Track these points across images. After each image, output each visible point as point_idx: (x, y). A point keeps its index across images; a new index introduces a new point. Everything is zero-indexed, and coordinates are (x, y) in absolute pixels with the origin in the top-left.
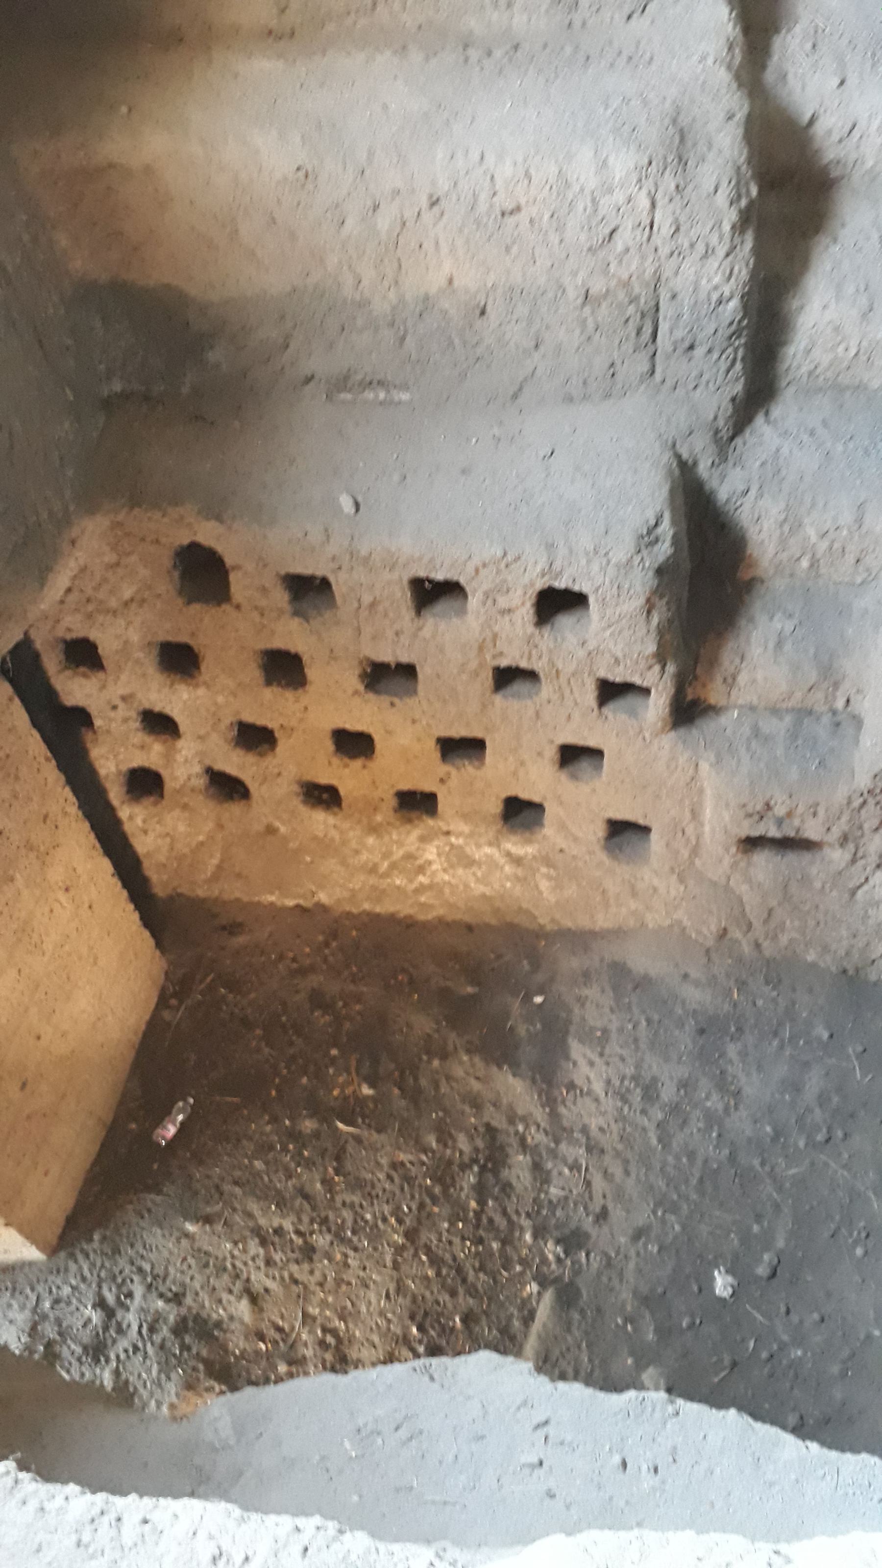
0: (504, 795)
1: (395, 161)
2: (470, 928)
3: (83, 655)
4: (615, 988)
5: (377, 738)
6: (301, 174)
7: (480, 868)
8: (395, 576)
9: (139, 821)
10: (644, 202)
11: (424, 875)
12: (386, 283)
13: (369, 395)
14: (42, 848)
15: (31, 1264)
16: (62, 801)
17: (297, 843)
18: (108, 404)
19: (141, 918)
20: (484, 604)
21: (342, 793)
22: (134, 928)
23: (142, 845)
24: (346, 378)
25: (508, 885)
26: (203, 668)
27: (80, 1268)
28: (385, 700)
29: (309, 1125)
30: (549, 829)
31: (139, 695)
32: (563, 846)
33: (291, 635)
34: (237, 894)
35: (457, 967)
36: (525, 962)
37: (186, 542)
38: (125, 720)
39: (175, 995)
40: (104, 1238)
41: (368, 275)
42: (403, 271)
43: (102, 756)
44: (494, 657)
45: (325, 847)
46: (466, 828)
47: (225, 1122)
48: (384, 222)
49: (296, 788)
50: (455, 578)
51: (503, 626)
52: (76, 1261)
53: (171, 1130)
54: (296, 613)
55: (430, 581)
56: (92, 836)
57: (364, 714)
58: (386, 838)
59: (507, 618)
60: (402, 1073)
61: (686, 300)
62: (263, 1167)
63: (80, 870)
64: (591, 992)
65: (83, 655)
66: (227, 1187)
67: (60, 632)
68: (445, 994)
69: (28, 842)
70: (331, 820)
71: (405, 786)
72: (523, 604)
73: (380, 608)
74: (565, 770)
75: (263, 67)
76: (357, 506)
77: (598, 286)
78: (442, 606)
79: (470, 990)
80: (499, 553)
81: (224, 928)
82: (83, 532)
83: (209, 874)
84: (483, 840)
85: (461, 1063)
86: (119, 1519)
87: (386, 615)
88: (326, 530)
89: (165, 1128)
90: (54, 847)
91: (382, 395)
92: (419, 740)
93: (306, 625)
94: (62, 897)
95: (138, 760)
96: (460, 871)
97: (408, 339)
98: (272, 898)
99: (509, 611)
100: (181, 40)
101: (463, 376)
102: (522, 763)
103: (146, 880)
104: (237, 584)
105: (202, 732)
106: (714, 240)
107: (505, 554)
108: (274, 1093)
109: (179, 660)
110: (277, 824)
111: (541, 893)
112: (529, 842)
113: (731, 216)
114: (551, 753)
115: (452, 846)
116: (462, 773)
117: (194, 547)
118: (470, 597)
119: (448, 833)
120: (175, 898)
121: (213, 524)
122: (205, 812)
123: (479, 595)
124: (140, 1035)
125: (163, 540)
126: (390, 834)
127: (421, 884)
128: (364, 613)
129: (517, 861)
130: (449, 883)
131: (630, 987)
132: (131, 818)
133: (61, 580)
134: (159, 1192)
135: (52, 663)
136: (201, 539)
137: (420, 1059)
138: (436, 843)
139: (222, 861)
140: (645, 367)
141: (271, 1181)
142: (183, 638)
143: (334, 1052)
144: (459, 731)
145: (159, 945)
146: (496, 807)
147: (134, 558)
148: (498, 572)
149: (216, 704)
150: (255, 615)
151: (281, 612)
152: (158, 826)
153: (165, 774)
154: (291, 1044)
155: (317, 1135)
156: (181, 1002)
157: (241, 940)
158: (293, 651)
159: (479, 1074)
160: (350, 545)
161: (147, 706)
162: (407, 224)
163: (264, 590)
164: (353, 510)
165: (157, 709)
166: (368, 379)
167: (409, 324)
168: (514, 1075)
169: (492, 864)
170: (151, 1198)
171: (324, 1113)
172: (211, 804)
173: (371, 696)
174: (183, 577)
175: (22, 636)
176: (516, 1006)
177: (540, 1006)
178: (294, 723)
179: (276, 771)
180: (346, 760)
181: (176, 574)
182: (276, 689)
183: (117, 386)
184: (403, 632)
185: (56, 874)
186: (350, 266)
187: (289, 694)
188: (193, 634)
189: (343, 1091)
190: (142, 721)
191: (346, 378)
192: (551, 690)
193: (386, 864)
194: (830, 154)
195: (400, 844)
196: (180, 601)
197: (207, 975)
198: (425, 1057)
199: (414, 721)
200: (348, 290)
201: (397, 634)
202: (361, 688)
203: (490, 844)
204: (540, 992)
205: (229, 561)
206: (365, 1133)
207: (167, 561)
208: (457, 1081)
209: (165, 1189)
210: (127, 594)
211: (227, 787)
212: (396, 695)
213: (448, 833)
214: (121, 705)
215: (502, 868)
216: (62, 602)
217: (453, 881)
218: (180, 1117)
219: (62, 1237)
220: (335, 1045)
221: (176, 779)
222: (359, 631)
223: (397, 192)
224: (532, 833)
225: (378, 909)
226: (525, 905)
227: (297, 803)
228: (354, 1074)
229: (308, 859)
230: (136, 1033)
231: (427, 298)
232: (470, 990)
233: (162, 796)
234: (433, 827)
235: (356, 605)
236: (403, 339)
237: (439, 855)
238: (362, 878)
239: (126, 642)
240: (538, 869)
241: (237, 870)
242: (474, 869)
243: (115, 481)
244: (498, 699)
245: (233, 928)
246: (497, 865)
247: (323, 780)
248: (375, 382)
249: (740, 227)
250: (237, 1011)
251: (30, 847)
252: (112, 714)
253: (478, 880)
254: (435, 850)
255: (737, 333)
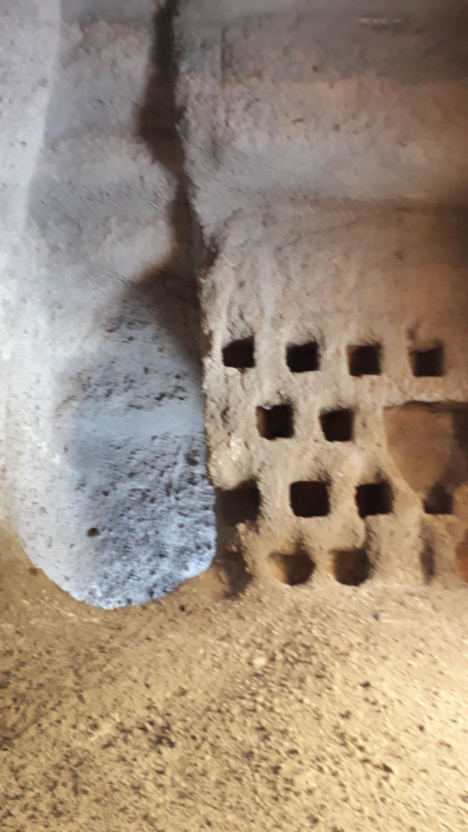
10: (232, 123)
13: (383, 21)
48: (364, 118)
61: (207, 73)
75: (413, 195)
77: (254, 81)
86: (131, 339)
106: (196, 103)
113: (189, 115)
140: (228, 35)
194: (142, 146)
223: (356, 133)
230: (335, 501)
249: (184, 109)
255: (180, 53)
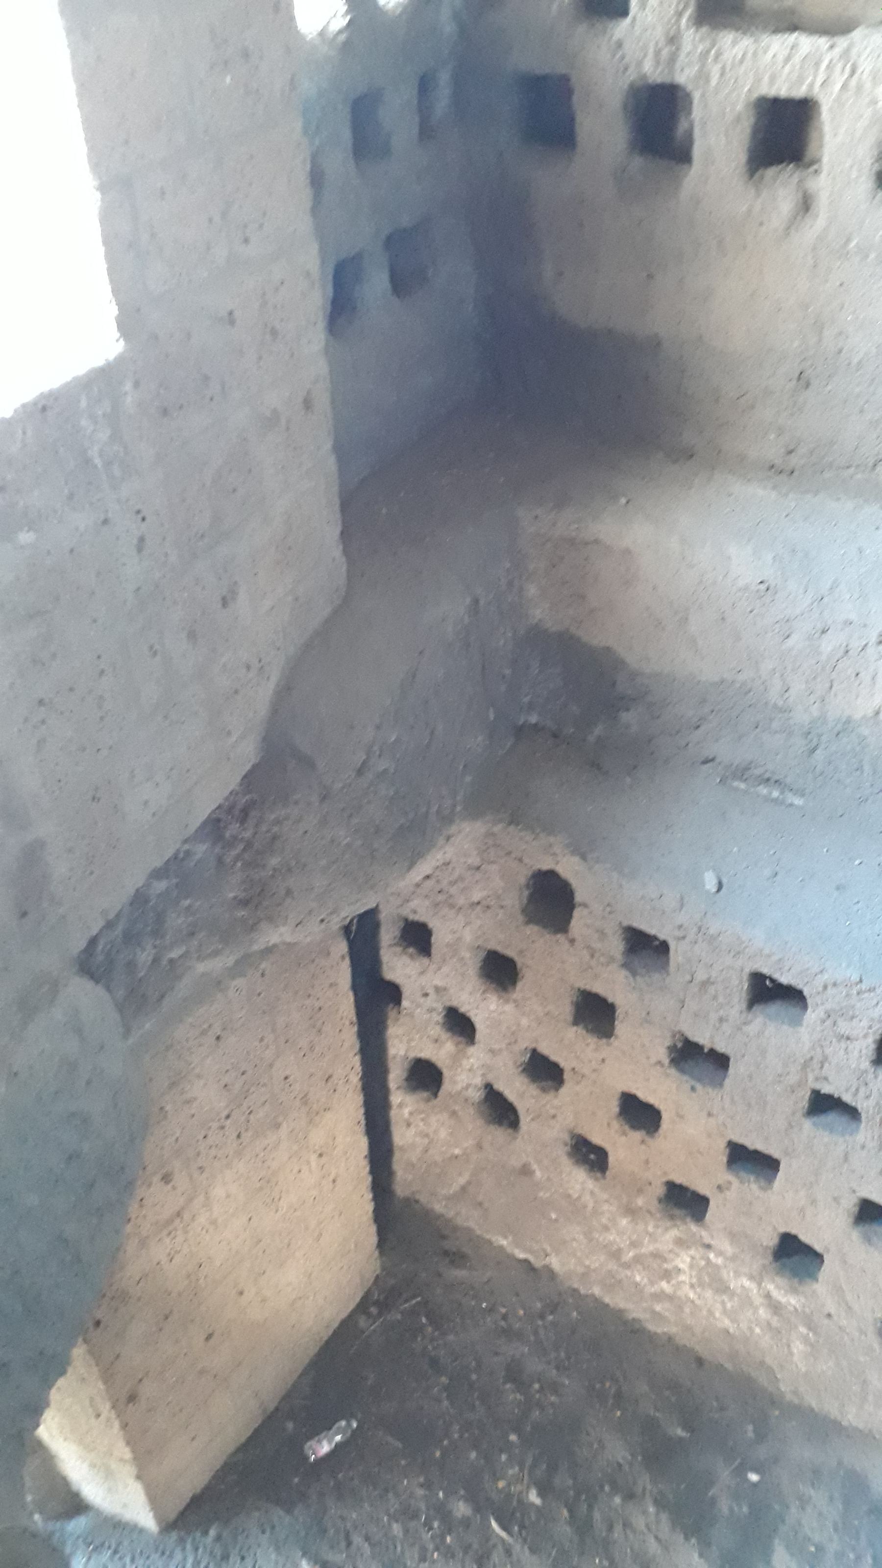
0: (783, 1230)
1: (856, 596)
2: (700, 1361)
3: (417, 937)
4: (847, 1502)
5: (665, 1116)
6: (763, 587)
7: (731, 1299)
8: (739, 963)
9: (406, 1111)
11: (668, 1282)
12: (812, 698)
13: (763, 790)
14: (315, 1106)
15: (142, 1531)
16: (349, 1068)
17: (548, 1195)
18: (520, 731)
19: (374, 1211)
20: (823, 1021)
21: (611, 1159)
22: (365, 1218)
23: (401, 1136)
24: (747, 769)
25: (758, 1330)
26: (520, 985)
27: (185, 1559)
28: (686, 1081)
29: (461, 1509)
30: (821, 1287)
31: (452, 991)
32: (833, 1312)
33: (615, 984)
34: (471, 1224)
35: (673, 1399)
36: (750, 1428)
37: (545, 867)
38: (431, 1010)
39: (376, 1303)
40: (218, 1538)
41: (798, 687)
42: (832, 693)
43: (397, 1036)
44: (817, 1079)
45: (575, 1209)
46: (728, 1248)
47: (380, 1464)
48: (828, 645)
49: (566, 1137)
50: (800, 986)
51: (836, 1051)
52: (184, 1549)
53: (325, 1448)
54: (625, 965)
55: (773, 980)
56: (362, 1111)
57: (661, 1088)
58: (641, 1227)
59: (843, 1045)
60: (578, 1494)
62: (401, 1535)
63: (339, 1140)
64: (818, 1497)
65: (417, 937)
66: (357, 1540)
67: (406, 912)
68: (650, 1426)
69: (306, 1095)
70: (590, 1184)
71: (679, 1179)
72: (865, 1036)
73: (712, 990)
74: (860, 1228)
75: (758, 494)
76: (720, 886)
78: (775, 1008)
79: (680, 1432)
80: (855, 978)
81: (446, 1253)
82: (460, 832)
83: (451, 1192)
84: (746, 1270)
85: (645, 1512)
87: (715, 998)
88: (682, 899)
89: (319, 1441)
90: (325, 1110)
91: (775, 794)
92: (709, 1136)
93: (631, 979)
94: (313, 1158)
95: (427, 1052)
96: (709, 1294)
97: (818, 752)
98: (504, 1243)
99: (848, 1038)
100: (692, 456)
101: (863, 800)
102: (814, 1202)
103: (391, 1173)
104: (579, 922)
105: (496, 1047)
107: (861, 981)
108: (438, 1454)
109: (500, 971)
110: (535, 1167)
111: (791, 1354)
112: (794, 1291)
114: (850, 1204)
115: (708, 1260)
116: (743, 1187)
117: (551, 875)
118: (810, 1010)
119: (708, 1247)
120: (410, 1202)
121: (576, 859)
122: (470, 1127)
123: (820, 1012)
124: (330, 1332)
125: (526, 860)
126: (646, 1224)
127: (663, 1292)
128: (694, 988)
129: (776, 1308)
130: (693, 1302)
131: (865, 1508)
132: (400, 1106)
133: (425, 867)
134: (289, 1511)
135: (388, 935)
136: (560, 870)
137: (602, 1487)
138: (692, 1252)
139: (469, 1183)
141: (403, 1552)
142: (510, 953)
143: (513, 1437)
144: (754, 1143)
145: (381, 1245)
146: (772, 1241)
147: (494, 868)
148: (848, 995)
149: (519, 1025)
150: (585, 953)
151: (612, 959)
152: (421, 1124)
153: (446, 1073)
154: (473, 1408)
155: (466, 1523)
156: (380, 1314)
157: (459, 1274)
158: (610, 1000)
159: (660, 1535)
160: (701, 920)
161: (455, 1003)
162: (850, 653)
163: (602, 934)
164: (714, 890)
165: (462, 1010)
166: (767, 776)
167: (824, 738)
168: (701, 1555)
169: (746, 1301)
170: (278, 1514)
171: (483, 1505)
172: (480, 1122)
173: (673, 1071)
174: (532, 898)
175: (374, 905)
176: (725, 1476)
177: (755, 1485)
178: (586, 1071)
179: (552, 1112)
180: (627, 1127)
181: (526, 893)
182: (580, 1030)
183: (533, 719)
184: (727, 1020)
185: (317, 1137)
186: (782, 675)
187: (592, 1040)
188: (521, 952)
189: (509, 1485)
190: (445, 1016)
191: (747, 769)
192: (869, 1137)
193: (631, 1254)
195: (653, 1237)
196: (521, 918)
197: (414, 1297)
198: (607, 1488)
199: (710, 1115)
200: (774, 695)
201: (721, 1020)
202: (666, 1061)
203: (751, 1278)
204: (756, 1470)
205: (578, 898)
206: (517, 1548)
207: (523, 876)
208: (634, 1531)
209: (296, 1512)
210: (476, 896)
211: (499, 1110)
212: (699, 1080)
213: (708, 1247)
214: (433, 995)
215: (756, 1309)
216: (418, 885)
217: (698, 1302)
218: (338, 1438)
219: (182, 1514)
220: (517, 1430)
221: (455, 1083)
222: (682, 1003)
224: (800, 1282)
225: (607, 1300)
226: (769, 1360)
227: (561, 1153)
228: (526, 1472)
229: (554, 1216)
231: (848, 721)
232: (680, 1432)
233: (435, 1095)
234: (694, 1234)
235: (688, 978)
236: (814, 750)
237: (691, 1266)
238: (602, 1258)
239: (459, 939)
240: (796, 1327)
241: (480, 1198)
242: (725, 1298)
243: (501, 796)
244: (808, 1124)
245: (457, 1258)
246: (751, 1304)
247: (596, 1139)
248: (772, 781)
250: (430, 1347)
251: (305, 1100)
252: (422, 1000)
253: (725, 1311)
254: (688, 1260)
